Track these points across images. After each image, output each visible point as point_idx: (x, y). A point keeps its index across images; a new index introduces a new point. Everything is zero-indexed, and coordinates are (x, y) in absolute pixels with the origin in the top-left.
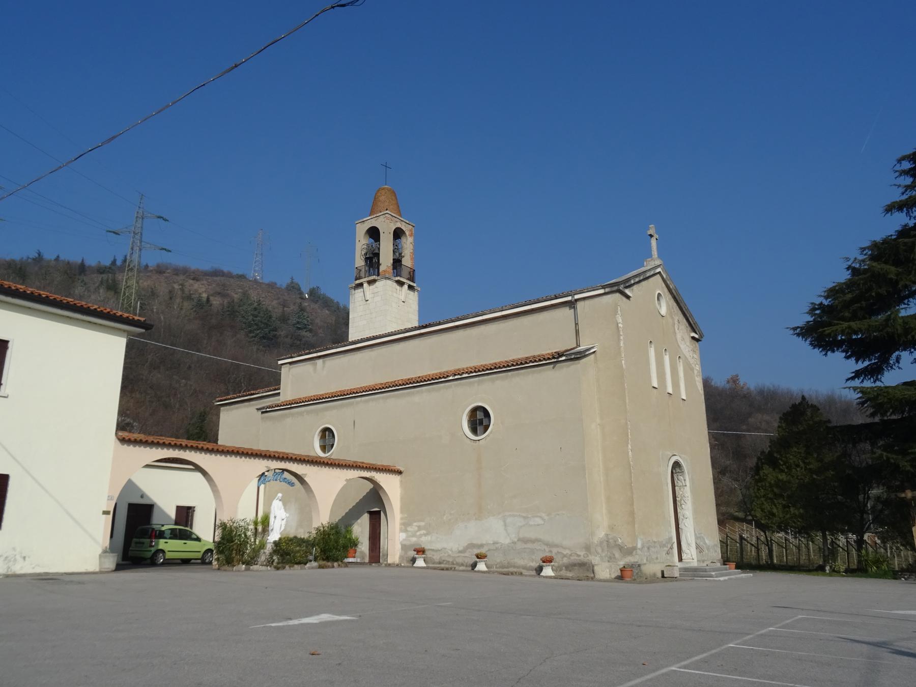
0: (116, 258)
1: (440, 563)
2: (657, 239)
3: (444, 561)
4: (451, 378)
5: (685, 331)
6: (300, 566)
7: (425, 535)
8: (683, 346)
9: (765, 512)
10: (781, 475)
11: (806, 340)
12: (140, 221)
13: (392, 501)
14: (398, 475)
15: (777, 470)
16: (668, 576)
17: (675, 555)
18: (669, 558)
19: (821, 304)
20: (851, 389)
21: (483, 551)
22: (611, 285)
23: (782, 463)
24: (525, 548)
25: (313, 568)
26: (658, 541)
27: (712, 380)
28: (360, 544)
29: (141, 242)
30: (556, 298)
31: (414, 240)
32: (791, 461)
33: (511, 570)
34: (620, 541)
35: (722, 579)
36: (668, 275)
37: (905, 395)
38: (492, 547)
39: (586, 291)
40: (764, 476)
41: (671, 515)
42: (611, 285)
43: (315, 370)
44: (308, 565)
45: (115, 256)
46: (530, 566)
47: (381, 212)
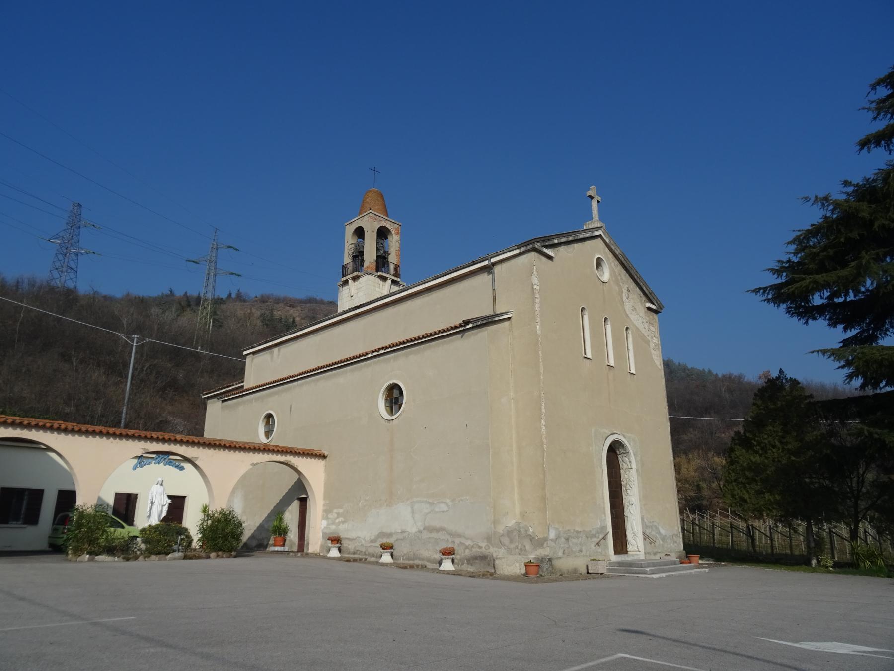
0: (231, 292)
1: (354, 553)
2: (598, 202)
3: (357, 551)
4: (370, 356)
5: (638, 300)
6: (158, 556)
7: (343, 522)
8: (633, 317)
9: (735, 498)
10: (754, 457)
11: (778, 306)
12: (214, 251)
13: (314, 490)
14: (323, 460)
15: (750, 452)
16: (593, 572)
17: (610, 548)
18: (600, 550)
19: (789, 261)
20: (820, 352)
21: (390, 541)
22: (526, 244)
23: (755, 443)
24: (429, 538)
25: (175, 559)
26: (584, 531)
27: (745, 376)
28: (289, 532)
29: (215, 269)
30: (474, 264)
31: (401, 239)
32: (766, 441)
33: (417, 562)
34: (531, 531)
35: (655, 576)
36: (611, 238)
37: (884, 355)
38: (400, 537)
39: (501, 252)
40: (735, 458)
41: (606, 501)
42: (526, 244)
43: (272, 358)
44: (170, 556)
45: (230, 291)
46: (434, 558)
47: (365, 212)
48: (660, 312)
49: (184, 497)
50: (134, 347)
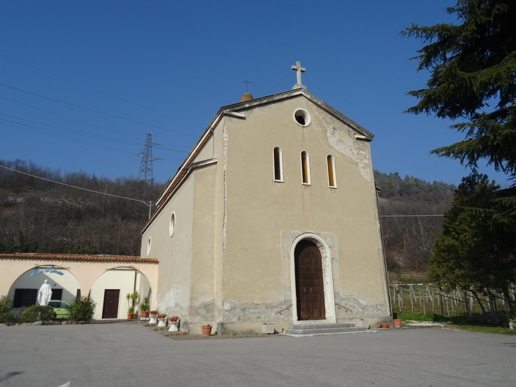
2: (302, 71)
25: (36, 325)
39: (213, 121)
48: (372, 140)
49: (119, 290)
50: (150, 208)
